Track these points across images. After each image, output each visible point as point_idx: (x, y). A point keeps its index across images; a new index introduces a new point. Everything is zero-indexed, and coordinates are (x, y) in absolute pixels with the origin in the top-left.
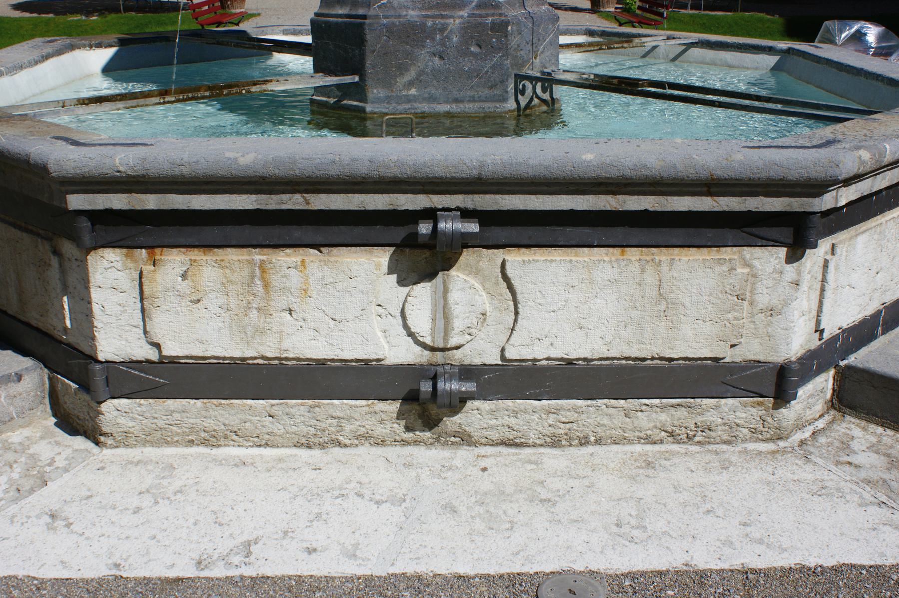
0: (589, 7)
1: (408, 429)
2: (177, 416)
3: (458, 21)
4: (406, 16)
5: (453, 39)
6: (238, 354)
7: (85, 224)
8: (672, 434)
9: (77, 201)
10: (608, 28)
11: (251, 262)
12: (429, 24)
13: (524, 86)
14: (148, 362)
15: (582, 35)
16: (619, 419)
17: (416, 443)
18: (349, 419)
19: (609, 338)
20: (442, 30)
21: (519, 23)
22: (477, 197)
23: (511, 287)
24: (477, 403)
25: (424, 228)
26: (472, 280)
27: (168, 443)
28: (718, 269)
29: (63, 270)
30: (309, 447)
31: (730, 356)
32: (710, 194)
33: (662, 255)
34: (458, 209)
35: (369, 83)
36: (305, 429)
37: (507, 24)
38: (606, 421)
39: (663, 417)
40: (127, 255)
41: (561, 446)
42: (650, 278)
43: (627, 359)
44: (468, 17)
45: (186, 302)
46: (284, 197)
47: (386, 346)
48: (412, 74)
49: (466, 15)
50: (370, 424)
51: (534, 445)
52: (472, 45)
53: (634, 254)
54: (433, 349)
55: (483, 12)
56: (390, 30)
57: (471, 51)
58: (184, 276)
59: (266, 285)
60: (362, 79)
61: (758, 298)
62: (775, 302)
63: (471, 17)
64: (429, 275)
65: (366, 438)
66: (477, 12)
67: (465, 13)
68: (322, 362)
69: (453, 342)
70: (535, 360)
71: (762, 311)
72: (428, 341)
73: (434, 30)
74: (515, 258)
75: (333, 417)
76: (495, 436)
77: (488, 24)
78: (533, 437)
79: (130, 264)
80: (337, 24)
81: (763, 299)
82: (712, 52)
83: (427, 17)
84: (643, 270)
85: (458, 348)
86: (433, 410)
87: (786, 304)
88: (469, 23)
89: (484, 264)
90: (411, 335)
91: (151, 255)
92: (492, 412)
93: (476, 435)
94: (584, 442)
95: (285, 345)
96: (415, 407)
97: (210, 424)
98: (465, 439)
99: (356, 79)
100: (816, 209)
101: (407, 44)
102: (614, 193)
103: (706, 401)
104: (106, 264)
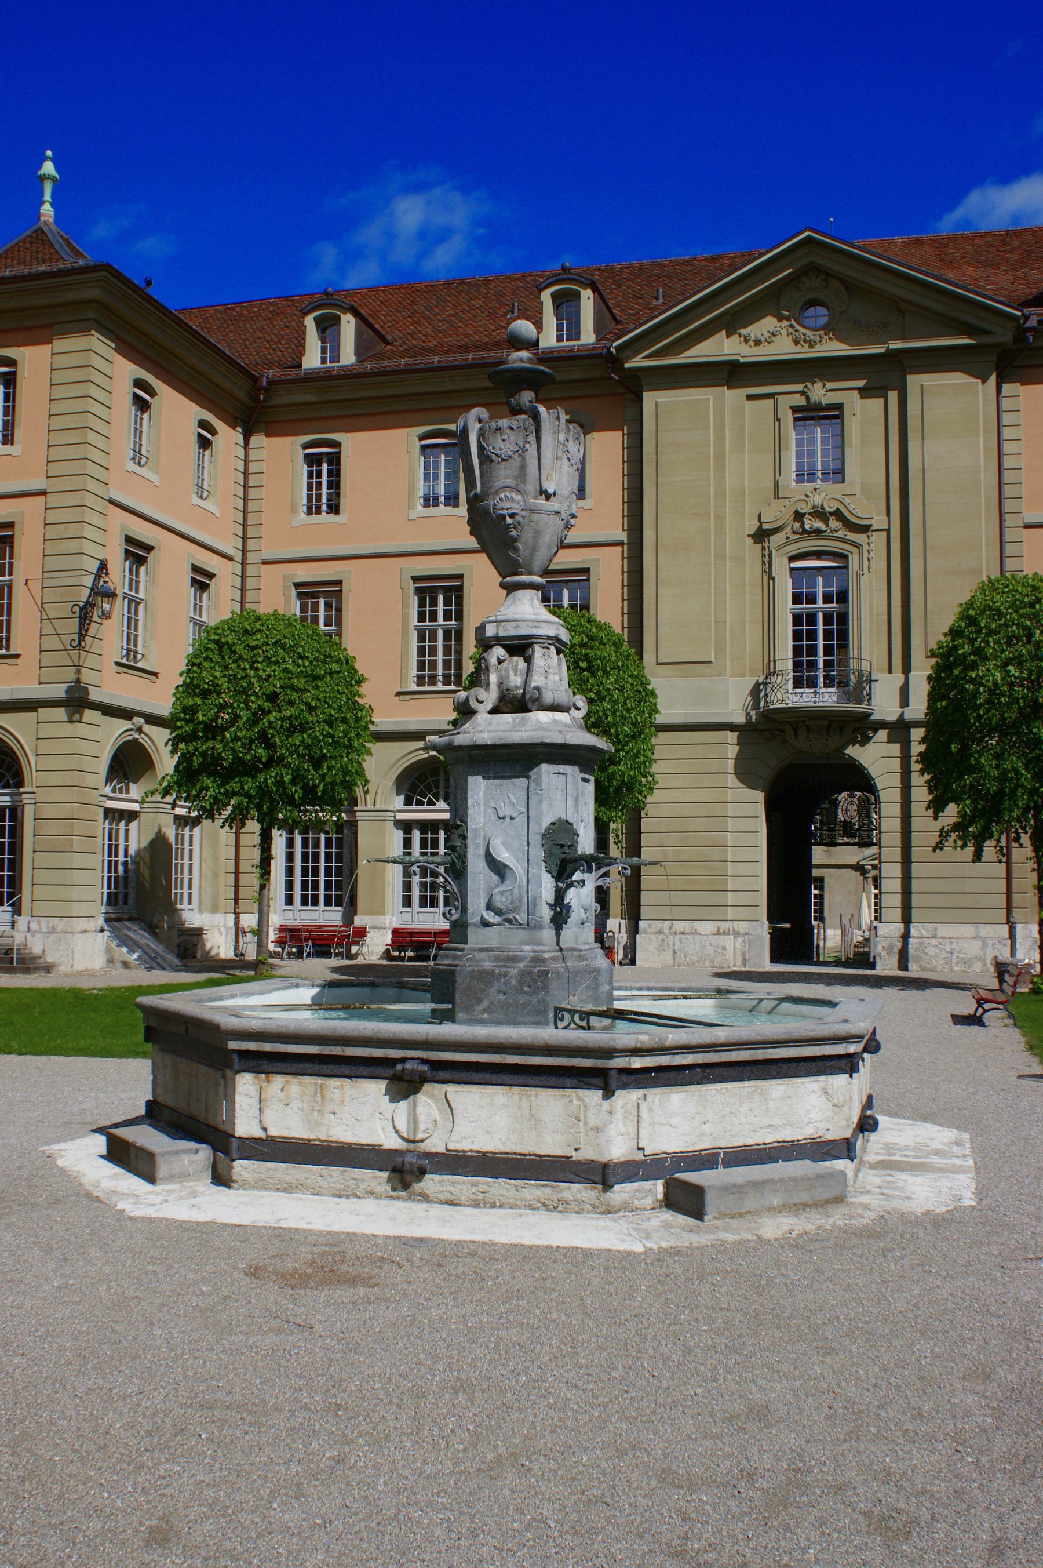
1: (394, 1189)
2: (272, 1172)
6: (306, 1137)
7: (235, 1057)
8: (544, 1205)
9: (233, 1045)
11: (316, 1084)
12: (497, 971)
13: (563, 1016)
14: (260, 1139)
16: (513, 1192)
17: (398, 1198)
18: (363, 1180)
19: (504, 1140)
20: (506, 975)
22: (429, 1053)
23: (450, 1106)
24: (432, 1176)
25: (399, 1067)
26: (429, 1101)
27: (266, 1189)
28: (562, 1101)
29: (225, 1087)
30: (340, 1197)
31: (576, 1156)
32: (550, 1055)
33: (532, 1091)
34: (418, 1059)
35: (457, 1009)
36: (338, 1185)
38: (505, 1193)
39: (538, 1193)
40: (255, 1077)
41: (480, 1207)
42: (525, 1105)
43: (515, 1154)
45: (281, 1105)
46: (333, 1048)
47: (382, 1135)
48: (485, 1004)
50: (374, 1185)
51: (464, 1205)
53: (516, 1090)
54: (409, 1141)
56: (473, 975)
58: (282, 1090)
59: (323, 1097)
60: (453, 1007)
61: (588, 1120)
62: (599, 1123)
64: (405, 1097)
65: (371, 1193)
67: (522, 965)
68: (349, 1145)
69: (419, 1136)
70: (464, 1151)
71: (592, 1129)
72: (405, 1135)
73: (500, 974)
74: (451, 1089)
75: (355, 1179)
76: (442, 1198)
78: (463, 1200)
79: (257, 1082)
80: (443, 970)
81: (592, 1122)
82: (795, 1006)
84: (521, 1100)
85: (422, 1141)
86: (408, 1178)
87: (605, 1125)
89: (436, 1092)
90: (397, 1132)
91: (267, 1077)
92: (440, 1182)
93: (432, 1196)
94: (493, 1206)
95: (330, 1133)
96: (398, 1175)
97: (289, 1178)
98: (425, 1198)
99: (450, 1006)
100: (611, 1066)
102: (499, 1053)
103: (561, 1184)
104: (244, 1081)
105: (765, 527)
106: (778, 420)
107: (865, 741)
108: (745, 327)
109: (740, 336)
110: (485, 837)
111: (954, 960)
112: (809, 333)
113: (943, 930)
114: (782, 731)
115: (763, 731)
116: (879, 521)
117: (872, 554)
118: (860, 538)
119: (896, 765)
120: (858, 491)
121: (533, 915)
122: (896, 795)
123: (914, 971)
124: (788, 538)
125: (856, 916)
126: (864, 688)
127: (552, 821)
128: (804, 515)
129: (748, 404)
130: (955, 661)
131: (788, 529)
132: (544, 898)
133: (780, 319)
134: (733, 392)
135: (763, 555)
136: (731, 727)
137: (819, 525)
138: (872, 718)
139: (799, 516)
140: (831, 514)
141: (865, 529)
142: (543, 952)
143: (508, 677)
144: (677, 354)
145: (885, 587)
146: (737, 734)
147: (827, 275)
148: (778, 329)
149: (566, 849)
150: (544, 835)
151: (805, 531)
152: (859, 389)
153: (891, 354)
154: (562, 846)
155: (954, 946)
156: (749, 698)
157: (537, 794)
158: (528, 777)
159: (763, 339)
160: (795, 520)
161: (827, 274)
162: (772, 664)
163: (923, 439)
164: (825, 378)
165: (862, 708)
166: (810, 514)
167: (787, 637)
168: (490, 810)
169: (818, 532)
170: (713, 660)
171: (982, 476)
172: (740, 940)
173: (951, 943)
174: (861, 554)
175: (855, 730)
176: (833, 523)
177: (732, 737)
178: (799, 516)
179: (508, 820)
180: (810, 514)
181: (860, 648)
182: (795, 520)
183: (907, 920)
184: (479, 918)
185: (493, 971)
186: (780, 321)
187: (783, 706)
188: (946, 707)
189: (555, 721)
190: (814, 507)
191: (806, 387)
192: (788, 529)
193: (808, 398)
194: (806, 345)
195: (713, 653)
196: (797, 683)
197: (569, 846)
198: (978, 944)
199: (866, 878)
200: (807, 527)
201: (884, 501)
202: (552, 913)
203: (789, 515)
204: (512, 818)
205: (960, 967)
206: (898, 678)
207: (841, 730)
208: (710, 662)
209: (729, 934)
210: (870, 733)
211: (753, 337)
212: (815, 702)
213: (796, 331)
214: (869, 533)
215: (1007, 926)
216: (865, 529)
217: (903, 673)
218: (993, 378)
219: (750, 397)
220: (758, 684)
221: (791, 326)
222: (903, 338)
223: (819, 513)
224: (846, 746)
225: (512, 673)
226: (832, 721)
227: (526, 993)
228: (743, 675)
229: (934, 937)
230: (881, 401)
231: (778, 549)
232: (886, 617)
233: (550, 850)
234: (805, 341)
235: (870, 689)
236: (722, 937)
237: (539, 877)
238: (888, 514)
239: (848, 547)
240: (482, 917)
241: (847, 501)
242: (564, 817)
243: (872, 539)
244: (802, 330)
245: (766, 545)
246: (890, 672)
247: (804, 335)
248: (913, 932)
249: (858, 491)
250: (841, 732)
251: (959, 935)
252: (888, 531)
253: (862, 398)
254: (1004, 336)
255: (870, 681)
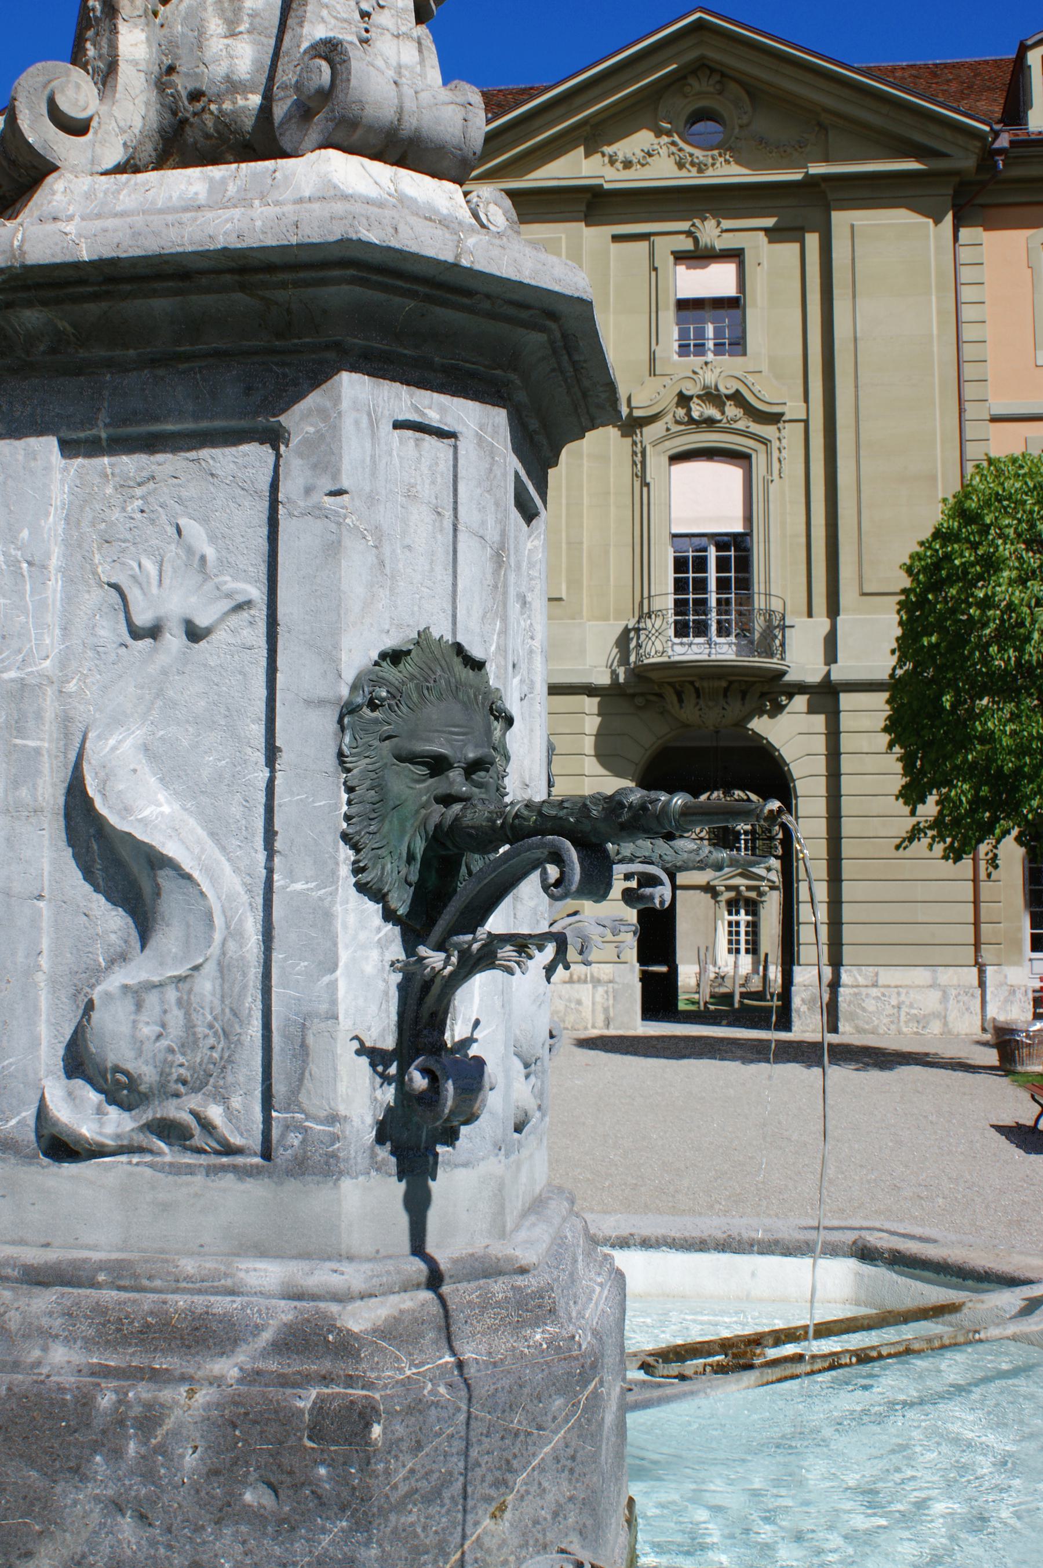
0: (997, 1063)
3: (204, 1396)
4: (38, 1364)
5: (182, 1456)
10: (912, 1237)
12: (106, 1401)
15: (844, 1256)
21: (417, 1407)
37: (366, 1414)
44: (241, 1381)
49: (234, 1373)
52: (244, 1483)
55: (295, 1366)
57: (247, 1506)
63: (251, 1383)
66: (272, 1365)
77: (301, 1411)
83: (106, 1372)
88: (236, 1404)
101: (31, 1463)
105: (637, 413)
106: (656, 269)
107: (777, 709)
108: (610, 144)
109: (603, 155)
110: (66, 721)
111: (903, 1018)
112: (697, 152)
113: (887, 976)
114: (660, 696)
115: (633, 696)
116: (794, 408)
117: (785, 453)
118: (767, 431)
119: (820, 744)
120: (764, 367)
121: (293, 1103)
122: (820, 786)
123: (848, 1034)
124: (668, 430)
125: (710, 949)
126: (776, 637)
127: (390, 642)
128: (691, 398)
129: (615, 247)
130: (949, 576)
131: (669, 418)
132: (346, 1025)
133: (659, 133)
134: (593, 230)
135: (634, 453)
136: (589, 690)
137: (712, 412)
138: (787, 678)
139: (683, 400)
140: (728, 397)
141: (774, 418)
142: (342, 1298)
143: (199, 43)
144: (520, 175)
145: (803, 499)
146: (597, 700)
147: (722, 75)
148: (656, 147)
149: (456, 781)
150: (349, 710)
151: (692, 421)
152: (766, 230)
153: (812, 183)
154: (438, 765)
155: (903, 998)
156: (615, 650)
157: (319, 513)
158: (274, 437)
159: (635, 160)
160: (678, 405)
161: (723, 75)
162: (646, 602)
163: (854, 297)
164: (720, 214)
165: (772, 663)
166: (699, 397)
167: (667, 567)
168: (94, 598)
169: (709, 422)
170: (564, 596)
171: (935, 349)
172: (601, 990)
173: (899, 994)
174: (769, 454)
175: (763, 695)
176: (732, 410)
177: (591, 704)
178: (683, 400)
179: (174, 640)
180: (699, 397)
181: (768, 582)
182: (678, 405)
183: (836, 962)
184: (29, 1114)
185: (85, 1401)
186: (658, 136)
187: (664, 659)
188: (937, 646)
189: (403, 201)
190: (705, 387)
191: (693, 225)
192: (669, 418)
193: (696, 241)
194: (694, 170)
195: (564, 587)
196: (681, 630)
197: (474, 767)
198: (936, 995)
199: (717, 902)
200: (695, 415)
201: (800, 381)
202: (388, 1094)
203: (671, 397)
204: (194, 634)
205: (913, 1027)
206: (821, 623)
207: (744, 695)
208: (560, 599)
209: (585, 982)
210: (784, 700)
211: (621, 157)
212: (709, 655)
213: (680, 150)
214: (781, 425)
215: (975, 970)
216: (774, 418)
217: (828, 616)
218: (949, 217)
219: (616, 238)
220: (626, 631)
221: (674, 144)
222: (827, 159)
223: (712, 396)
224: (749, 717)
225: (215, 26)
226: (731, 683)
227: (256, 1517)
228: (607, 619)
229: (875, 985)
230: (796, 246)
231: (655, 444)
232: (803, 540)
233: (379, 786)
234: (693, 164)
235: (784, 636)
236: (576, 986)
237: (326, 917)
238: (806, 400)
239: (751, 443)
240: (42, 1113)
241: (750, 379)
242: (441, 630)
243: (784, 433)
244: (688, 149)
245: (638, 439)
246: (810, 615)
247: (691, 155)
248: (845, 977)
249: (764, 367)
250: (743, 698)
251: (909, 983)
252: (806, 422)
253: (770, 242)
254: (966, 162)
255: (784, 628)
